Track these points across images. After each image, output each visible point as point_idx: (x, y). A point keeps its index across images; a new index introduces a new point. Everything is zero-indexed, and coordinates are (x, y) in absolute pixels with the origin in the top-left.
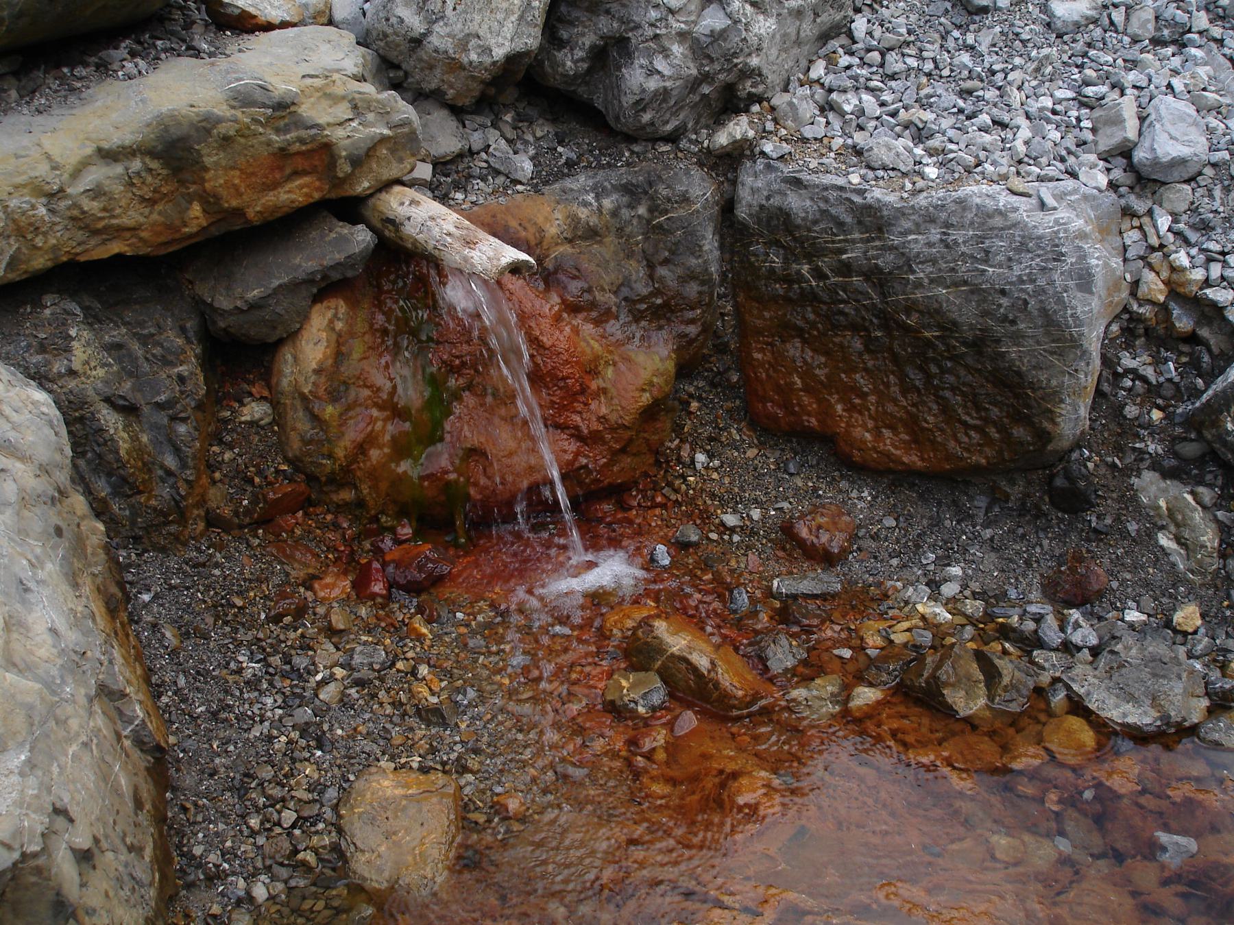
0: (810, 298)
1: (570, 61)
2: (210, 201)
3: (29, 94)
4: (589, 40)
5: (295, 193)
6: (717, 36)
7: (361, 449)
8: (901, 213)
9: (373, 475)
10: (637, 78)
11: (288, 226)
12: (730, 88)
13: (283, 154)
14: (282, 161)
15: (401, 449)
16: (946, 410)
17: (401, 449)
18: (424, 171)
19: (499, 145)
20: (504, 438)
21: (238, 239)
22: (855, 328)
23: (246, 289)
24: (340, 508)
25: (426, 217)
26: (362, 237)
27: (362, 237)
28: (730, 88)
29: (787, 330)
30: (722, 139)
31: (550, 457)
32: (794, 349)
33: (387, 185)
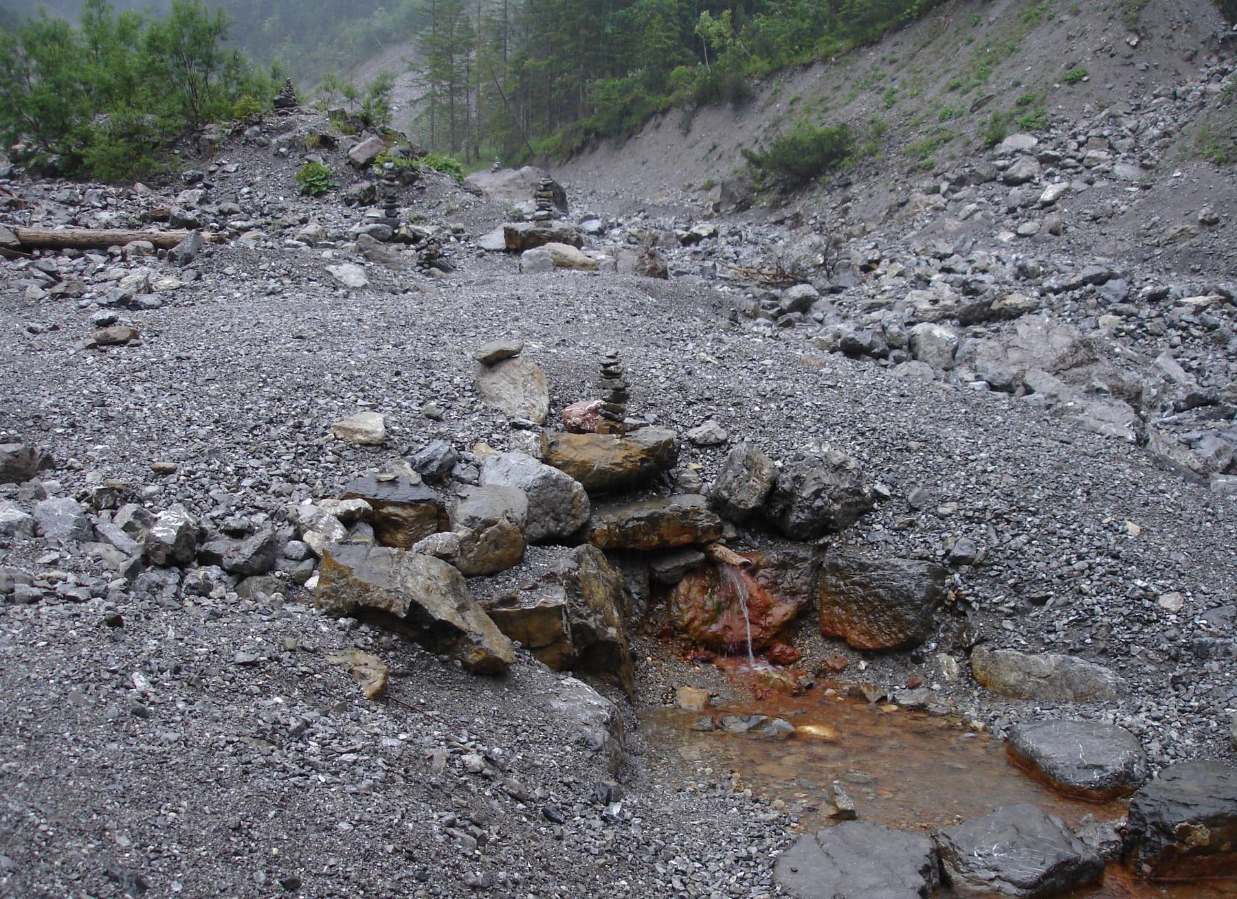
0: (842, 592)
1: (775, 512)
2: (660, 536)
3: (635, 500)
4: (781, 506)
5: (685, 538)
6: (820, 508)
7: (692, 620)
8: (870, 565)
9: (695, 629)
10: (793, 518)
11: (679, 550)
12: (825, 526)
13: (683, 526)
14: (683, 529)
15: (705, 623)
16: (880, 628)
17: (705, 623)
18: (724, 541)
19: (748, 537)
20: (737, 624)
21: (666, 551)
22: (855, 602)
23: (666, 567)
24: (682, 639)
25: (721, 551)
26: (702, 556)
27: (702, 556)
28: (825, 526)
29: (836, 603)
30: (821, 542)
31: (749, 632)
32: (837, 609)
33: (712, 542)
